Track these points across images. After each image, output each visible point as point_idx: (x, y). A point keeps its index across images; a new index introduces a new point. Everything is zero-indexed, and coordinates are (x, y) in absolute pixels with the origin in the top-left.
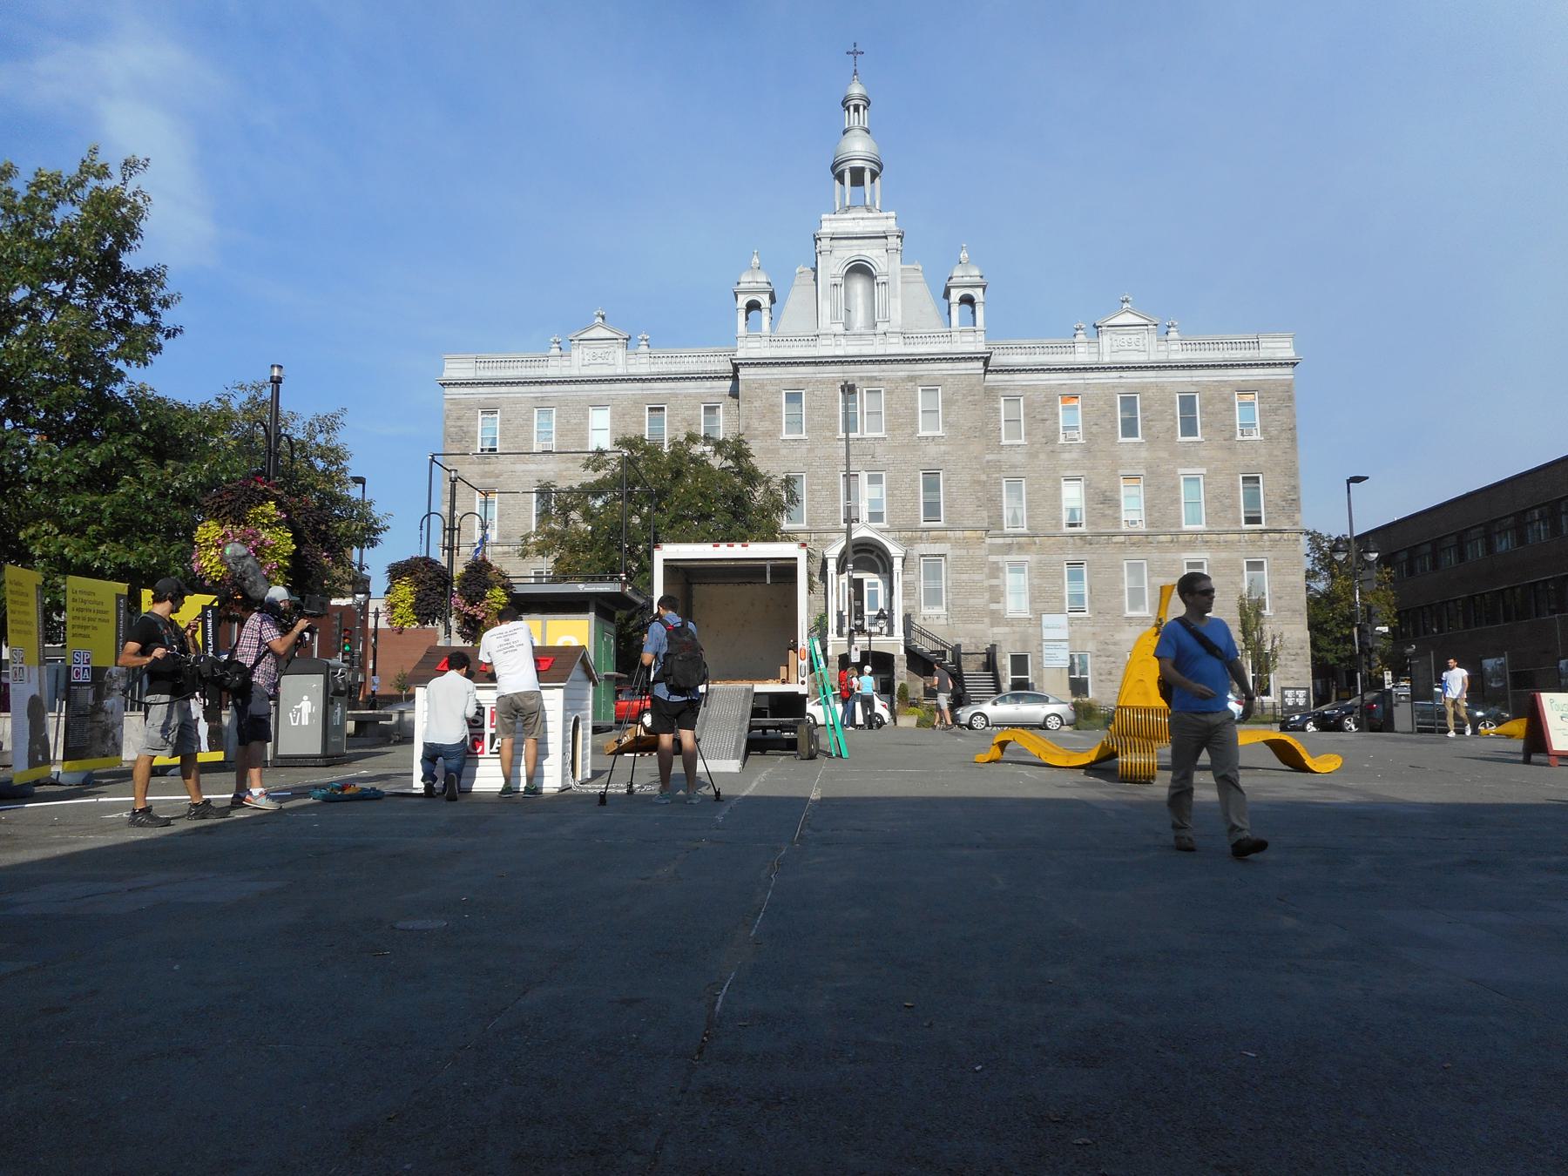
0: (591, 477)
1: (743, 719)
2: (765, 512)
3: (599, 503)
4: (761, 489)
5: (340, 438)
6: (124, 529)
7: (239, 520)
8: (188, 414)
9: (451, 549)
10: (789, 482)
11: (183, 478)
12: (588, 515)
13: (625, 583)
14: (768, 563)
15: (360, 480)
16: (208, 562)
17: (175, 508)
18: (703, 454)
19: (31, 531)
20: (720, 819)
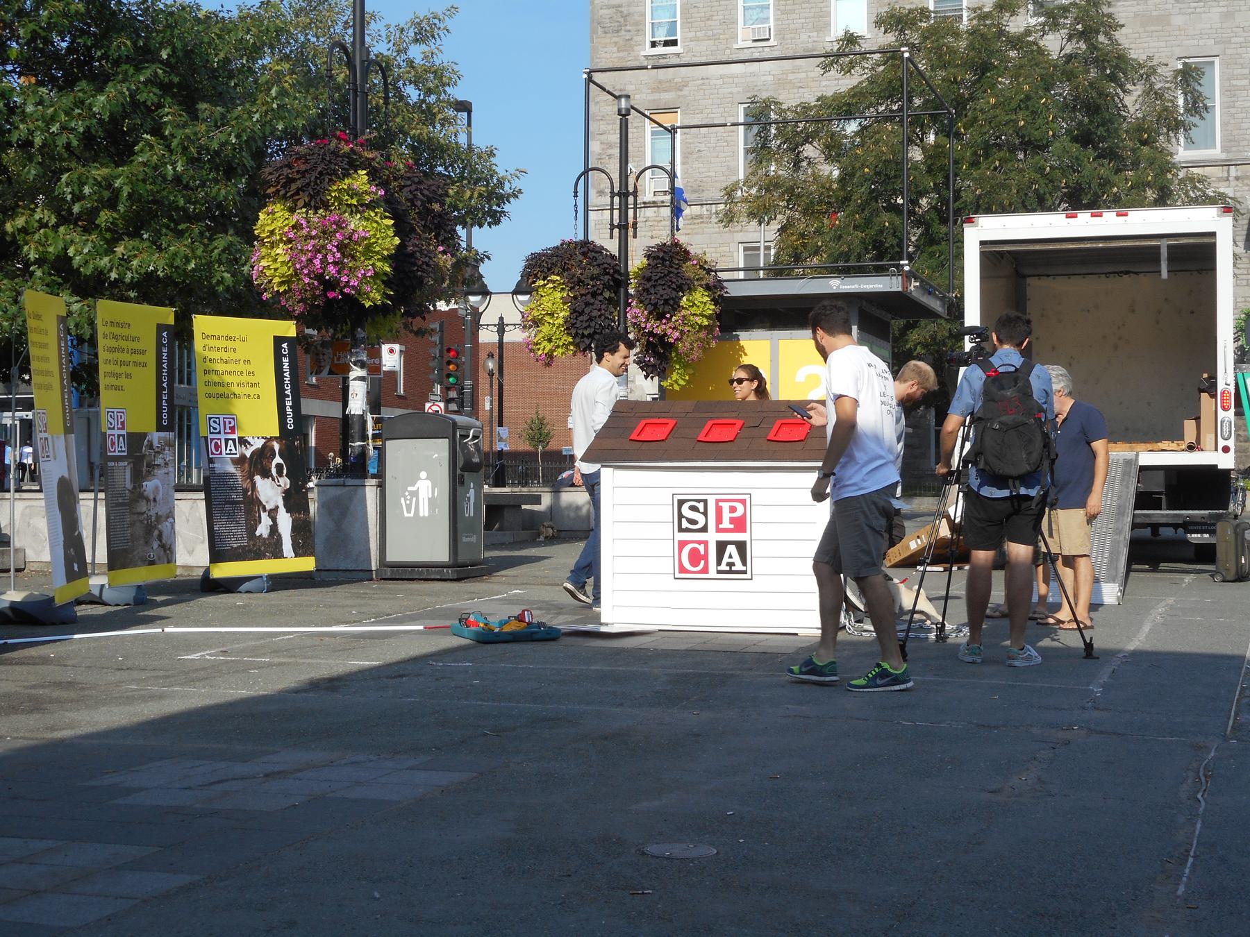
0: (839, 83)
1: (1121, 512)
2: (1144, 135)
3: (852, 127)
4: (1137, 90)
5: (448, 51)
6: (145, 218)
7: (317, 202)
8: (227, 27)
9: (623, 228)
10: (1189, 76)
11: (218, 133)
12: (834, 150)
13: (908, 277)
14: (1164, 244)
15: (464, 107)
16: (271, 265)
17: (216, 181)
18: (1028, 32)
19: (20, 222)
20: (1096, 689)
